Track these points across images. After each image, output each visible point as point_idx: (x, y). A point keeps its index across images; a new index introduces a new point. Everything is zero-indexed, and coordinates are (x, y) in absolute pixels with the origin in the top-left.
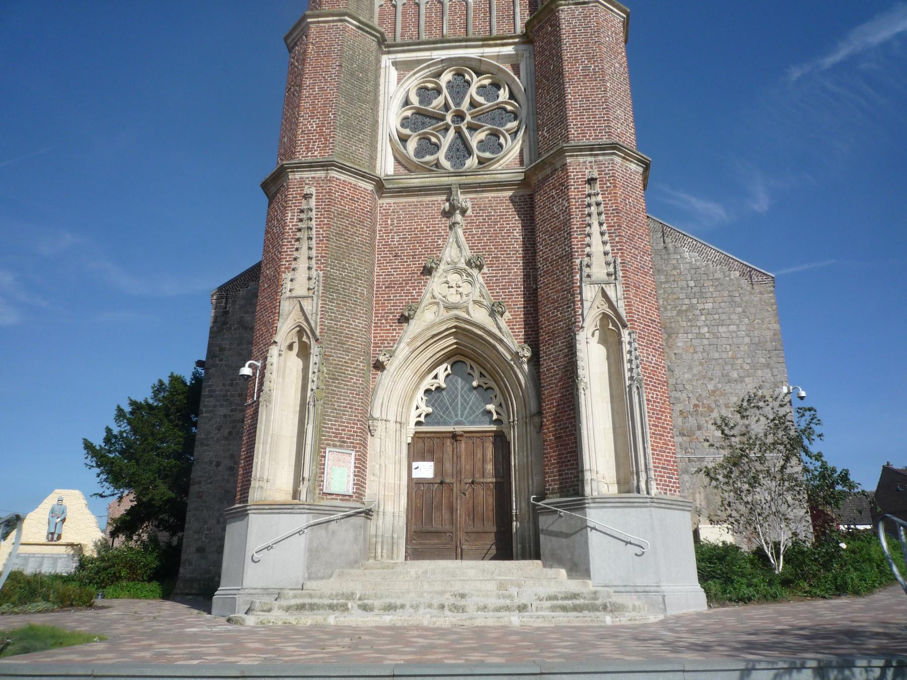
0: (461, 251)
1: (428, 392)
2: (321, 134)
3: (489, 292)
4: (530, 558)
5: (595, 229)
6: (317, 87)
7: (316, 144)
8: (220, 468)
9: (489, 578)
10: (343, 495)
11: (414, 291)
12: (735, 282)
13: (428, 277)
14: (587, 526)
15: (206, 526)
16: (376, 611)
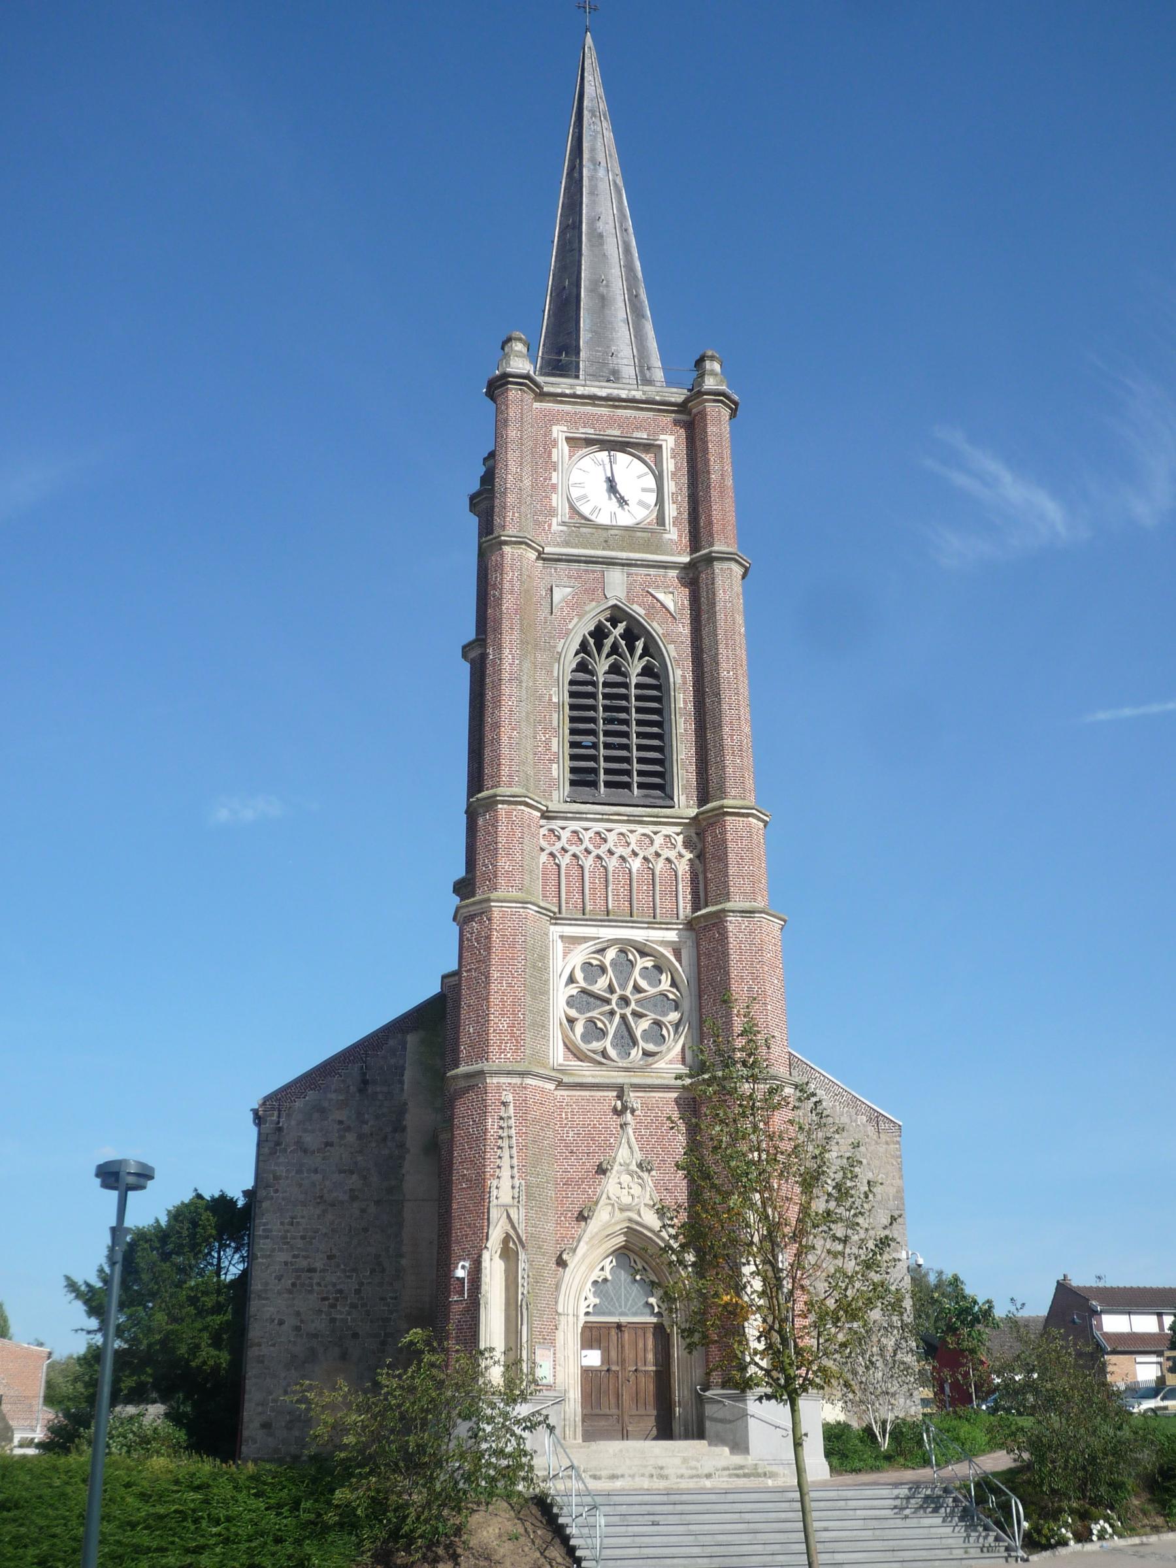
0: (632, 1152)
1: (595, 1283)
2: (512, 1035)
3: (657, 1195)
4: (693, 1438)
6: (504, 982)
7: (508, 1045)
8: (285, 1327)
9: (670, 1454)
10: (547, 1386)
11: (590, 1190)
12: (862, 1128)
13: (602, 1176)
14: (747, 1414)
15: (270, 1397)
16: (603, 1480)
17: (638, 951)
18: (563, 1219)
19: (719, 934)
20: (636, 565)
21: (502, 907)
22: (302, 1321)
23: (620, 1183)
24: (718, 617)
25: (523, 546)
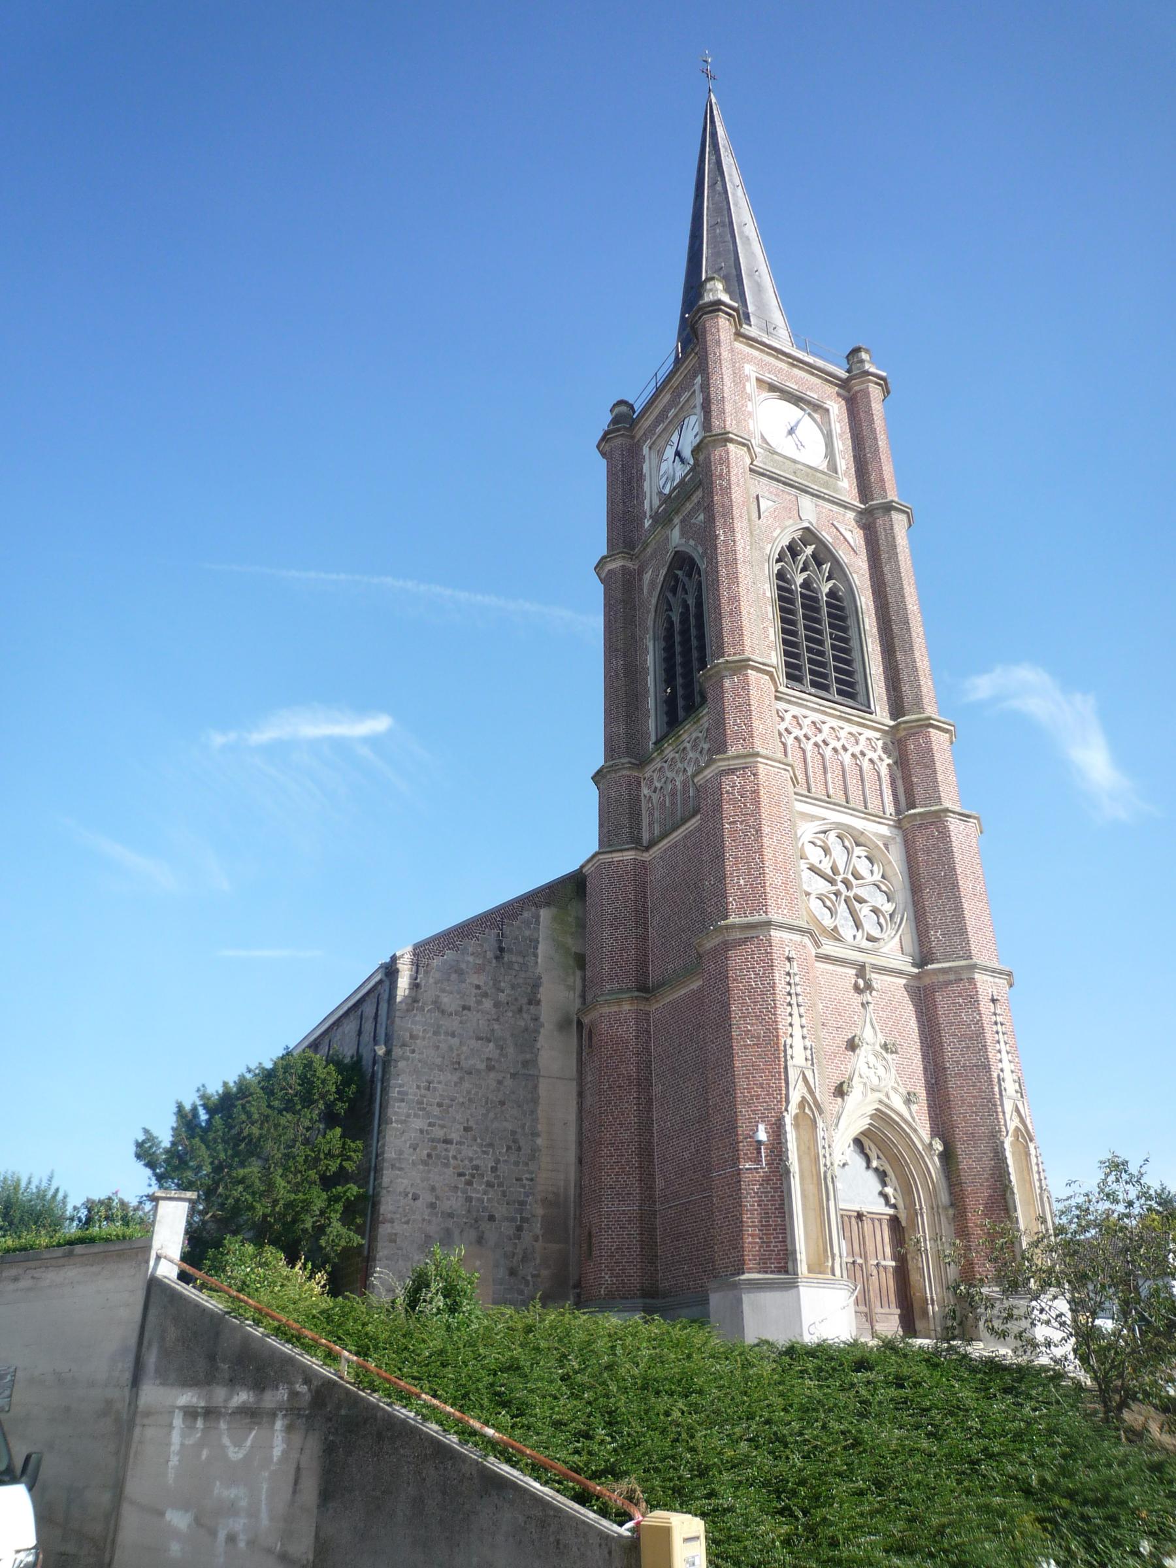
0: (875, 1032)
8: (419, 1203)
20: (823, 499)
21: (766, 764)
22: (437, 1198)
24: (900, 558)
25: (745, 449)
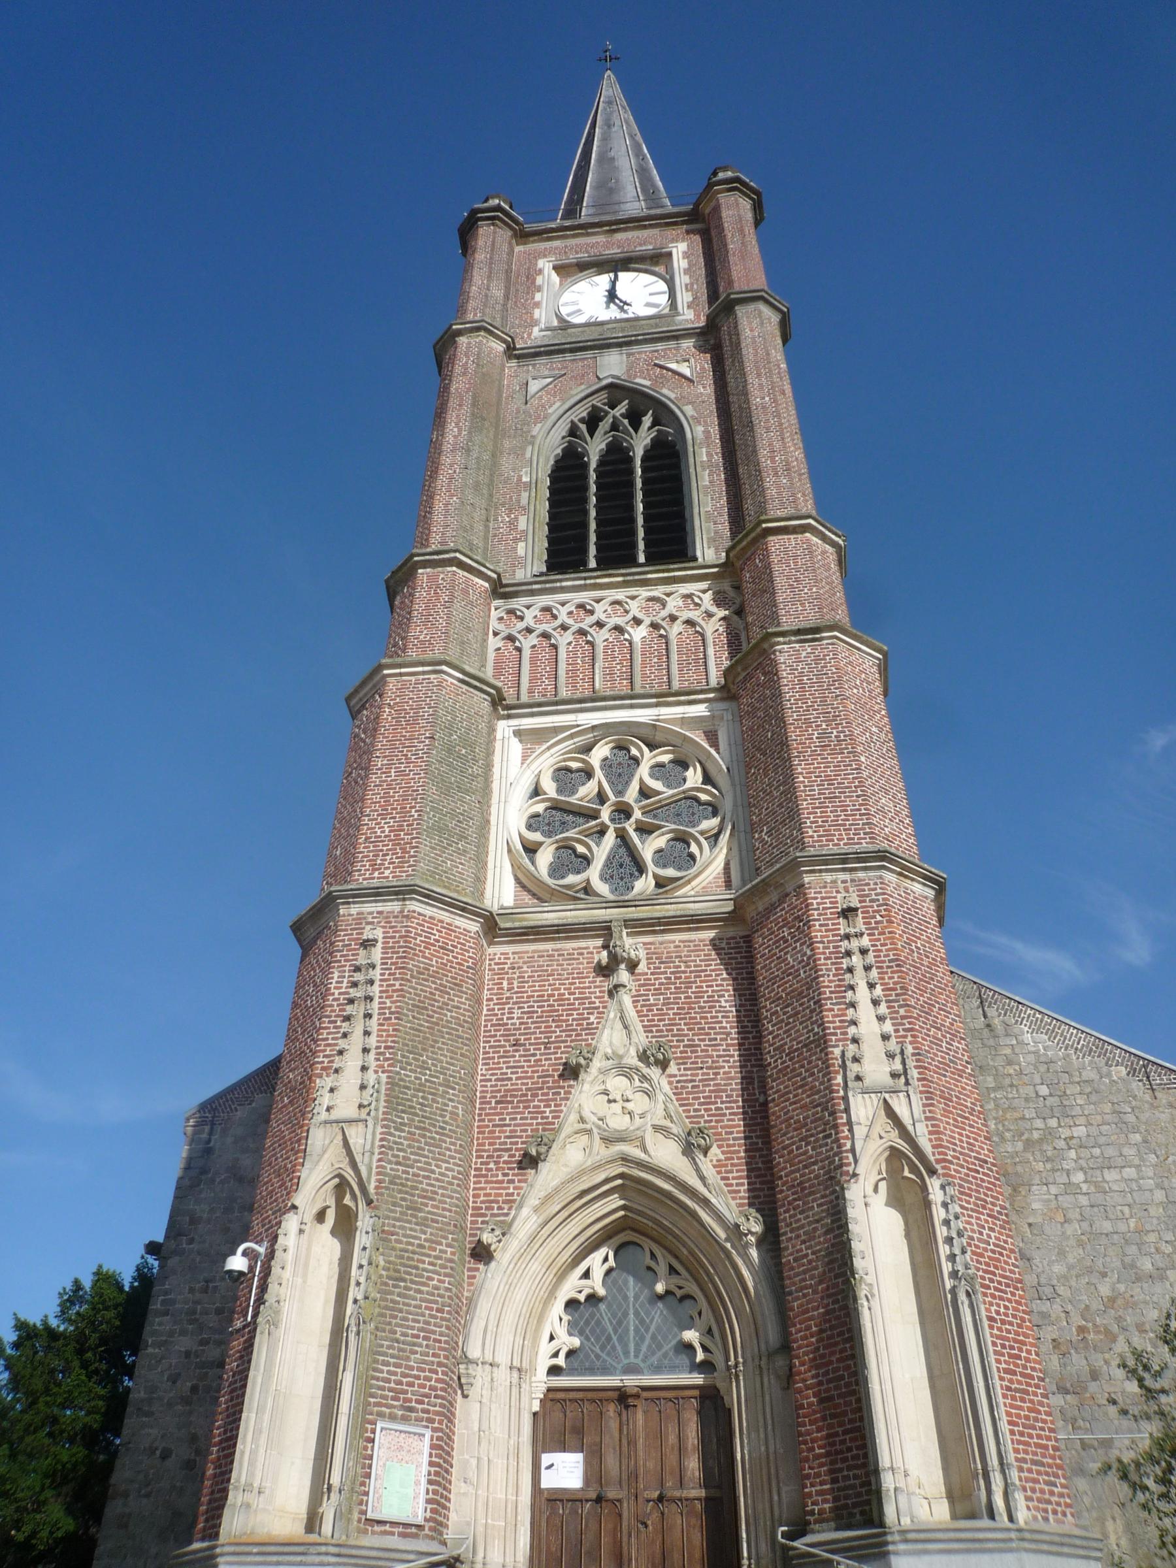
0: (629, 1035)
1: (571, 1304)
3: (681, 1109)
5: (862, 995)
7: (388, 858)
10: (406, 1525)
11: (548, 1110)
12: (1121, 1086)
13: (572, 1082)
17: (647, 745)
18: (492, 1166)
19: (765, 674)
20: (638, 342)
21: (401, 675)
23: (606, 1093)
24: (744, 352)
25: (482, 333)
